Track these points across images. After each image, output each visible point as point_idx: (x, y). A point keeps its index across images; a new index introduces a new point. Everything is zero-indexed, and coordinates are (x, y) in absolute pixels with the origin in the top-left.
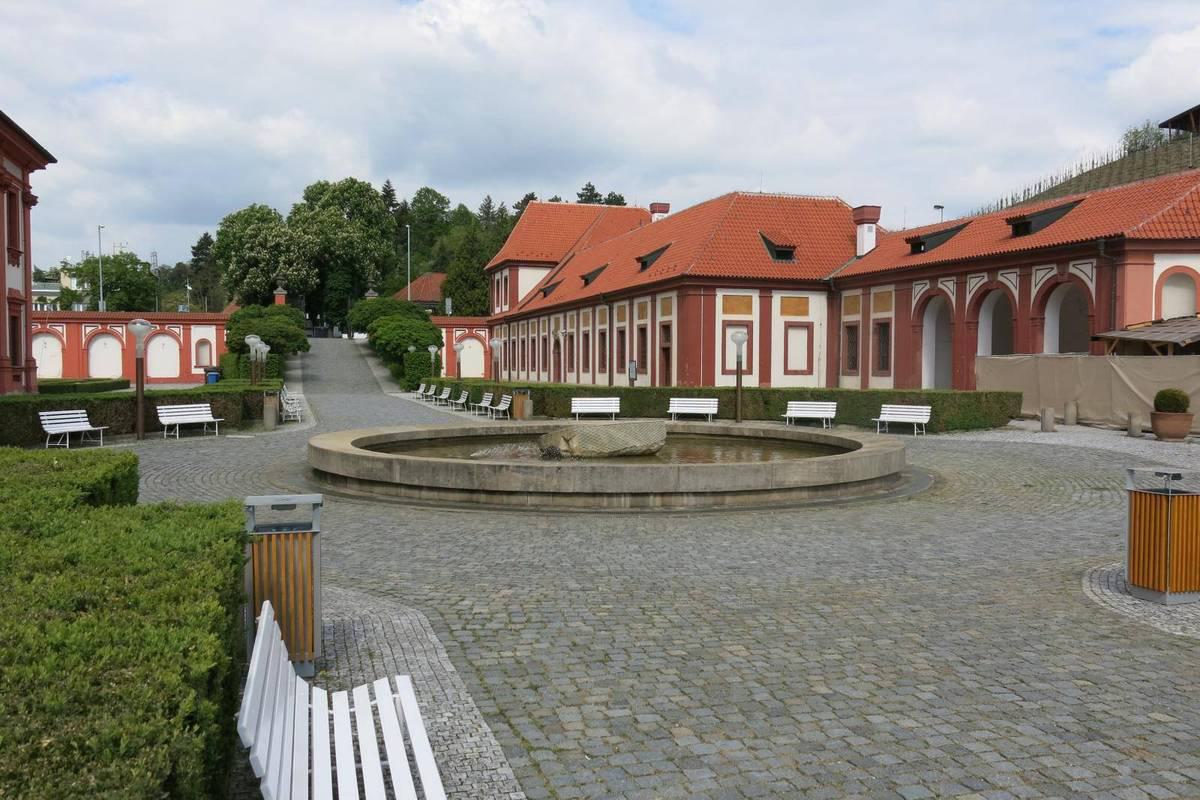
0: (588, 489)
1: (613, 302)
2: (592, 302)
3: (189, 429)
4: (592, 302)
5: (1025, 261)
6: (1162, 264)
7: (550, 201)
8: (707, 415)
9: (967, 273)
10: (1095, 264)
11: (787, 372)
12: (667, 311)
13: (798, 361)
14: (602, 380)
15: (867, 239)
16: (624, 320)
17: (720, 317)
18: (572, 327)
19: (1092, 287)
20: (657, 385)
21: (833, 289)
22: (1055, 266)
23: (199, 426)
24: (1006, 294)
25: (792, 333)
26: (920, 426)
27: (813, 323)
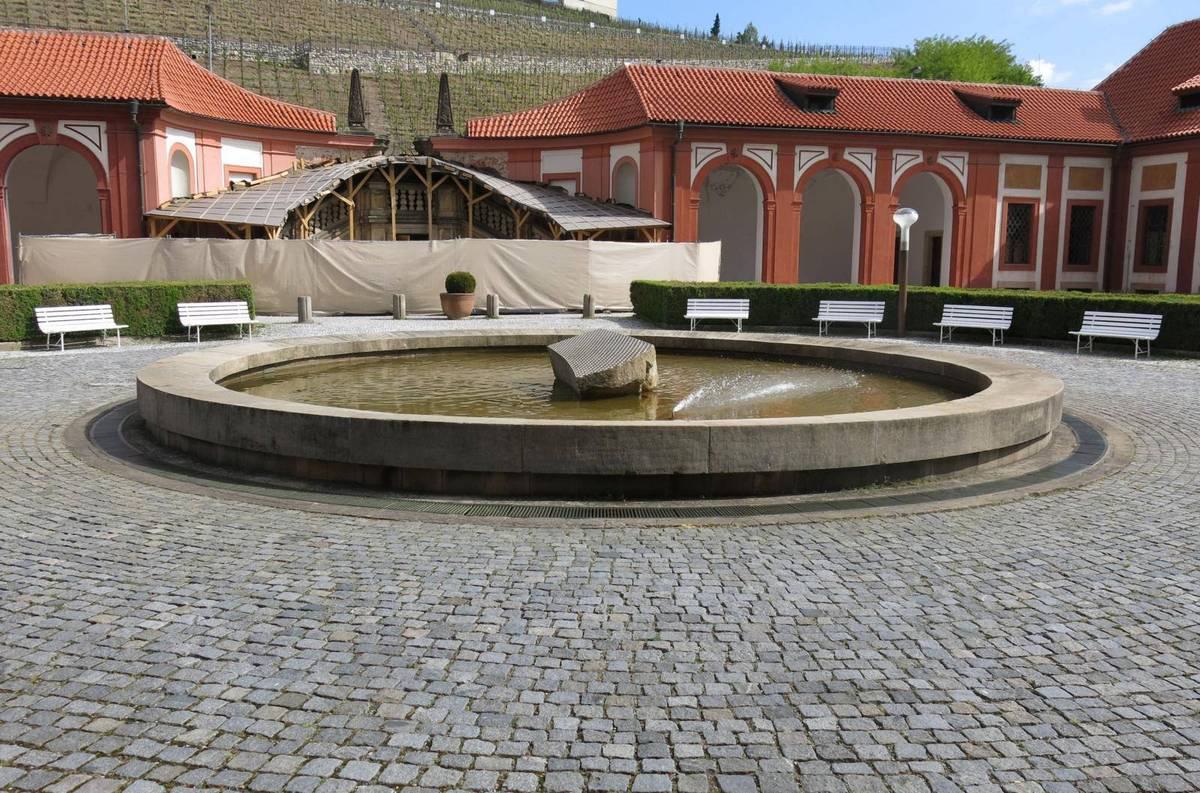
3: (82, 339)
8: (736, 320)
10: (874, 155)
19: (103, 156)
23: (97, 334)
26: (1143, 343)
27: (1103, 201)
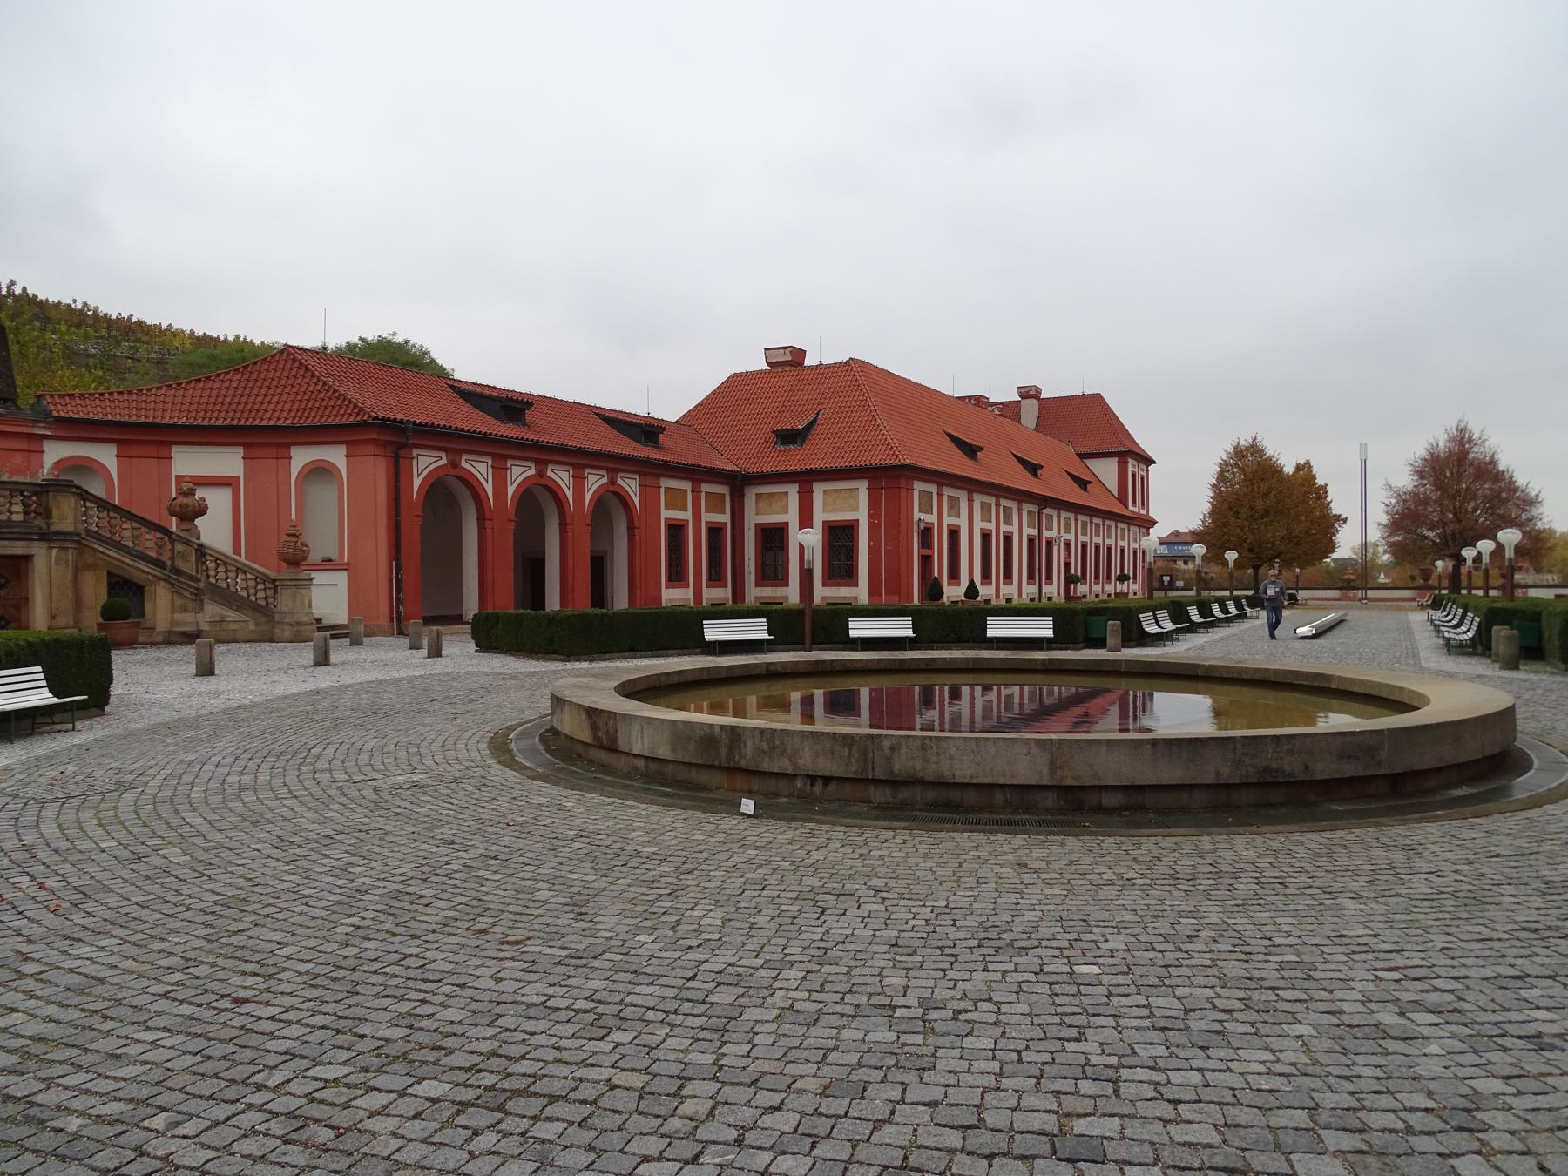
6: (301, 457)
22: (443, 455)
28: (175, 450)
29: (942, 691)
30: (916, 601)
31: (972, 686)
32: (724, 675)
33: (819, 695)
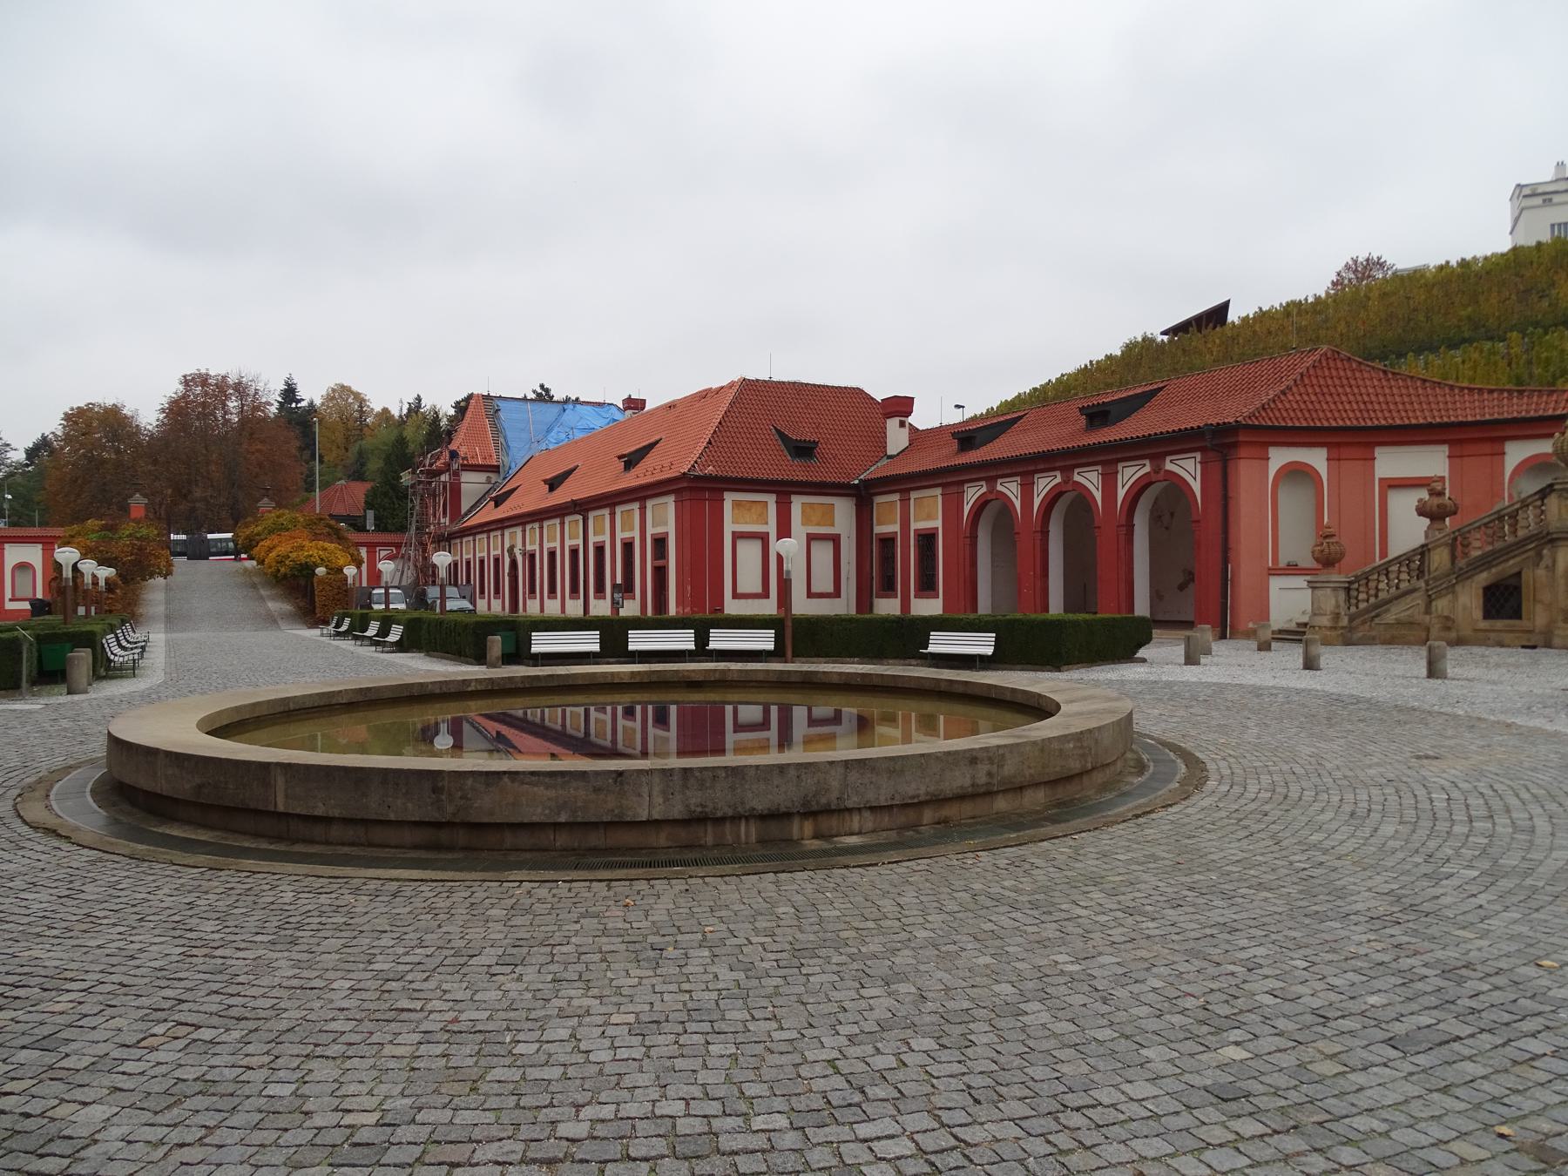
0: (677, 812)
1: (588, 510)
2: (560, 512)
4: (560, 512)
5: (1109, 457)
6: (1279, 458)
7: (223, 728)
9: (963, 482)
11: (810, 595)
12: (627, 526)
13: (823, 582)
14: (574, 609)
15: (897, 439)
16: (632, 529)
17: (729, 528)
18: (532, 543)
19: (1196, 487)
20: (650, 613)
21: (863, 496)
22: (1147, 462)
24: (1084, 496)
25: (815, 546)
28: (1379, 452)
29: (644, 712)
30: (1056, 607)
31: (644, 705)
32: (1008, 697)
33: (620, 709)
